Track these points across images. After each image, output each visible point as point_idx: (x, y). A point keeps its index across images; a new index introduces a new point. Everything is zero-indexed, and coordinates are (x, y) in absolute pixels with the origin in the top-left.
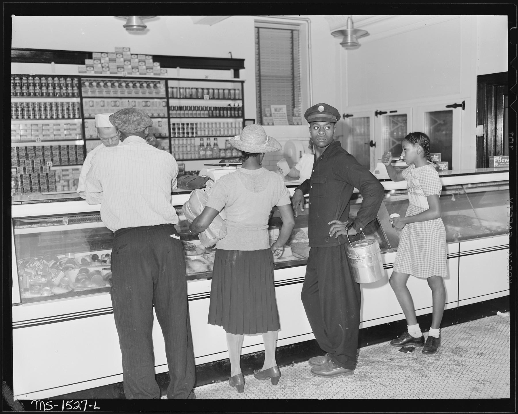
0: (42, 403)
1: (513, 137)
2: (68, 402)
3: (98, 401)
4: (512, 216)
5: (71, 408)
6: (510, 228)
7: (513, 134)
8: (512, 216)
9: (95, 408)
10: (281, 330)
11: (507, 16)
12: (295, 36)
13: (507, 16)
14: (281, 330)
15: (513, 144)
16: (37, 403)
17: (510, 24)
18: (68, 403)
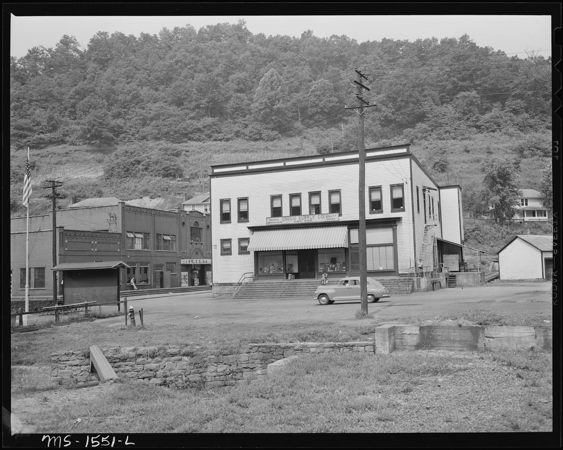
0: (58, 440)
1: (557, 146)
2: (93, 438)
3: (130, 435)
4: (556, 231)
5: (48, 437)
6: (554, 244)
7: (557, 143)
8: (556, 231)
9: (126, 443)
10: (230, 222)
11: (550, 16)
12: (393, 273)
13: (550, 16)
14: (230, 222)
15: (558, 154)
16: (55, 440)
17: (554, 24)
18: (94, 440)
